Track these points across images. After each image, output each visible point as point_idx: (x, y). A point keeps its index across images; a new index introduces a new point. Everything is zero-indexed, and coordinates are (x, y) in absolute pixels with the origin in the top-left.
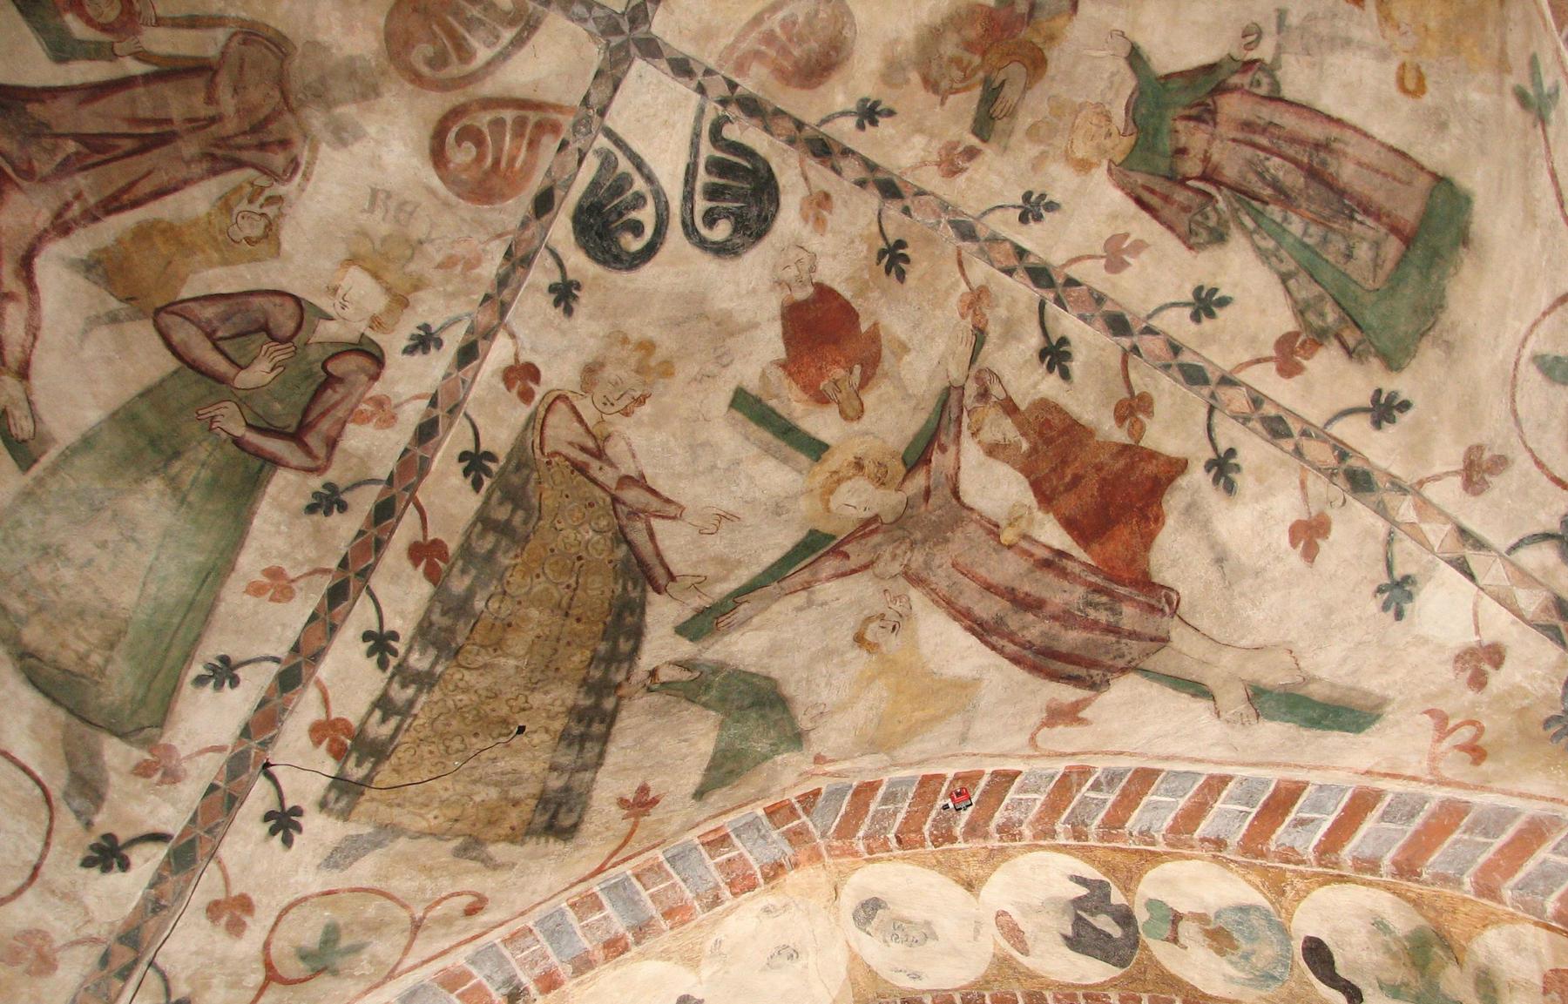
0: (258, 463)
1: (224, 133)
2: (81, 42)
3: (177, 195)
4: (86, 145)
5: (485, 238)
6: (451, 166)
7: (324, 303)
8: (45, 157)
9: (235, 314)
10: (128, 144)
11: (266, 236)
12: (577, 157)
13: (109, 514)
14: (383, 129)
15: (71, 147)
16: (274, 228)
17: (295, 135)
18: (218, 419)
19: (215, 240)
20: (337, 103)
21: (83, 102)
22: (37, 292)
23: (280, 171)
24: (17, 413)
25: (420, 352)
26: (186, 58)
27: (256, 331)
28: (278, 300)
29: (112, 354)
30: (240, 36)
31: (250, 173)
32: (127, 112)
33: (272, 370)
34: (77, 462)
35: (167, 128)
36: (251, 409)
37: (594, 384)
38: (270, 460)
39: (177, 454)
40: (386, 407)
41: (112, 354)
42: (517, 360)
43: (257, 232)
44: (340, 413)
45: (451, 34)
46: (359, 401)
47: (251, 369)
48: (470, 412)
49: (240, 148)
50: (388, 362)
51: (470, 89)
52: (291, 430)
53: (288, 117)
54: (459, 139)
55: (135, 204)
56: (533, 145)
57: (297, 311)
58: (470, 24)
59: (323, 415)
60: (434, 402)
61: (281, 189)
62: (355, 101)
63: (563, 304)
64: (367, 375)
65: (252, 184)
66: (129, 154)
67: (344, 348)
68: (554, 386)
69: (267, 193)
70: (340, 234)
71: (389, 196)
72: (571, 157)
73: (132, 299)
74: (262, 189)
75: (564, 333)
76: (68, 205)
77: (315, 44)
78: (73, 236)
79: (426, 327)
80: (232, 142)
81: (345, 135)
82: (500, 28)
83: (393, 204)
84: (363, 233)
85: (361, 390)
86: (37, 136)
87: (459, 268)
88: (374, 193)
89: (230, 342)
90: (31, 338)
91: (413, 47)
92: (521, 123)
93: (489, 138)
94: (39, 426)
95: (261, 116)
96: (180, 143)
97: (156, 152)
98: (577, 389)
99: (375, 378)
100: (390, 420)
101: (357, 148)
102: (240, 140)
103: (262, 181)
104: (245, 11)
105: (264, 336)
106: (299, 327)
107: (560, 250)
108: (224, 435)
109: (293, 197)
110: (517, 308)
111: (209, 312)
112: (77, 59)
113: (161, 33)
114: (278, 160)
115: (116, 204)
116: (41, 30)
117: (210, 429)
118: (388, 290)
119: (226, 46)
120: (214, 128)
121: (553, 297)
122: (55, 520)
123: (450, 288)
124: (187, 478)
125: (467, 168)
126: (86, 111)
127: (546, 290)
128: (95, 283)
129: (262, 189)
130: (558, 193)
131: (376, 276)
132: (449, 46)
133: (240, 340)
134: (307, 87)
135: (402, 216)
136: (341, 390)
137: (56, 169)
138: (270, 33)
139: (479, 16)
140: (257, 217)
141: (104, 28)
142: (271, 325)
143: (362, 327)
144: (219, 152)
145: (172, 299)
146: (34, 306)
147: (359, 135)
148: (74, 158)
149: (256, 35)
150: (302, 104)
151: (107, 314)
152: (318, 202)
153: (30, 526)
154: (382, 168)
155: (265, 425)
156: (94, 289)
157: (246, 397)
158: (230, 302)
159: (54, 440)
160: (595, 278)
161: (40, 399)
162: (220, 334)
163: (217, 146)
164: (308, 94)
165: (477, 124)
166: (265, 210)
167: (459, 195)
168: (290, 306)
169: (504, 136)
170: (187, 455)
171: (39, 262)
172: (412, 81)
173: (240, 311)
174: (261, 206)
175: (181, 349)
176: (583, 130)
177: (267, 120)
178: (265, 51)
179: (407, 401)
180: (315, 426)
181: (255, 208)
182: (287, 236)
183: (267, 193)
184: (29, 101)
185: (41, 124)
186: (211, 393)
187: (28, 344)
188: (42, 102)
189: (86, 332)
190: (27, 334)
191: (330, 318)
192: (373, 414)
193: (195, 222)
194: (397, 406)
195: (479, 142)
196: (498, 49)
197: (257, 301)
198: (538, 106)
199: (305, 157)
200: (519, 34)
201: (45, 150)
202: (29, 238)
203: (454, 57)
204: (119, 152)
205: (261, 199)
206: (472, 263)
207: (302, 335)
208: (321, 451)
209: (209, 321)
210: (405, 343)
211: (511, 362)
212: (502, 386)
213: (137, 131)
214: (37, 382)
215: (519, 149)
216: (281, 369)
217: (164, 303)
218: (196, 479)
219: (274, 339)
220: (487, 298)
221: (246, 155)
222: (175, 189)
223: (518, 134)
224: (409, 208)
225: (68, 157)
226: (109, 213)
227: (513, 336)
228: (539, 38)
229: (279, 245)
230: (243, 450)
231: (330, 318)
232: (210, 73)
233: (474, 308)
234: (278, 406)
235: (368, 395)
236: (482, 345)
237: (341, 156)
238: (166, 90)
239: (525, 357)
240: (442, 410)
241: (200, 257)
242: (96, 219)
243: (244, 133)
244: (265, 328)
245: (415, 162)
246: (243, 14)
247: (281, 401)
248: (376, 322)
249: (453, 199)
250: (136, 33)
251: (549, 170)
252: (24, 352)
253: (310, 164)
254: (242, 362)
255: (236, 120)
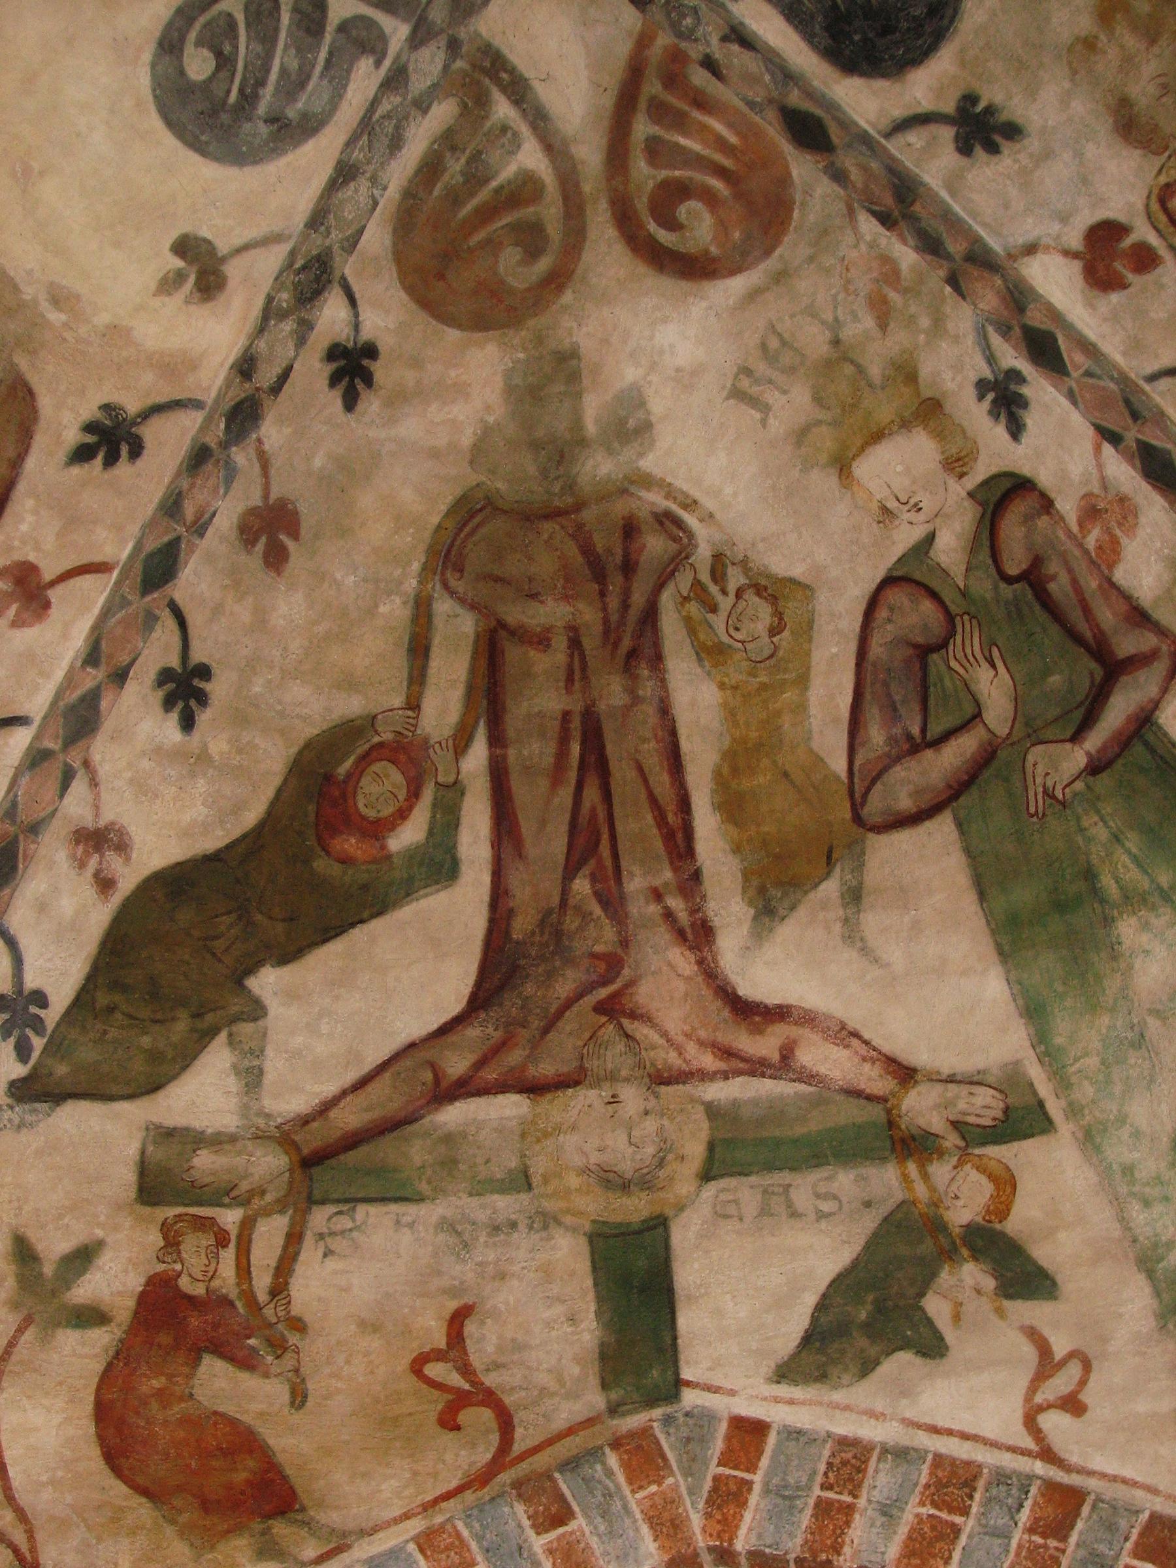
0: (1138, 748)
1: (598, 629)
2: (431, 833)
3: (683, 733)
4: (582, 862)
5: (850, 238)
6: (714, 250)
7: (905, 536)
8: (592, 931)
9: (889, 695)
10: (592, 794)
11: (774, 600)
12: (735, 48)
13: (1153, 1023)
14: (632, 354)
15: (582, 886)
16: (763, 582)
17: (620, 508)
18: (1049, 784)
19: (764, 687)
20: (577, 425)
21: (520, 854)
22: (789, 1007)
23: (674, 547)
24: (962, 1105)
25: (1021, 412)
26: (473, 670)
27: (924, 668)
28: (882, 614)
29: (906, 919)
30: (449, 574)
31: (667, 599)
32: (544, 784)
33: (993, 666)
34: (1059, 1040)
35: (576, 724)
36: (1047, 725)
37: (1156, 128)
38: (1141, 727)
39: (1089, 875)
40: (1101, 505)
41: (906, 919)
42: (1075, 255)
43: (764, 613)
44: (1091, 583)
45: (487, 213)
46: (1081, 546)
47: (983, 698)
48: (1149, 370)
49: (625, 606)
50: (1026, 471)
51: (587, 188)
52: (1099, 673)
53: (588, 515)
54: (673, 225)
55: (684, 804)
56: (701, 102)
57: (909, 588)
58: (475, 178)
59: (1086, 610)
60: (1113, 438)
61: (703, 553)
62: (579, 395)
63: (998, 139)
64: (1039, 515)
65: (686, 599)
66: (607, 796)
67: (986, 534)
68: (1140, 205)
69: (705, 577)
70: (796, 473)
71: (747, 371)
72: (736, 58)
73: (829, 857)
74: (697, 584)
75: (1047, 155)
76: (669, 915)
77: (478, 453)
78: (716, 922)
79: (982, 387)
80: (614, 618)
81: (631, 423)
82: (488, 124)
83: (761, 368)
84: (801, 435)
85: (1061, 534)
86: (558, 934)
87: (893, 296)
88: (737, 394)
89: (931, 719)
90: (855, 1042)
91: (502, 282)
92: (660, 112)
93: (677, 173)
94: (991, 1080)
95: (580, 559)
96: (602, 706)
97: (609, 748)
98: (1158, 161)
99: (1047, 504)
100: (1126, 509)
101: (657, 406)
102: (613, 603)
103: (684, 581)
104: (409, 563)
105: (935, 657)
106: (934, 595)
107: (898, 113)
108: (1079, 786)
109: (718, 536)
110: (985, 225)
111: (876, 736)
112: (455, 846)
113: (430, 705)
114: (655, 545)
115: (680, 836)
116: (407, 891)
117: (1063, 804)
118: (905, 425)
119: (462, 601)
120: (586, 642)
121: (979, 151)
122: (1139, 1111)
123: (925, 322)
124: (1133, 875)
125: (722, 226)
126: (532, 850)
127: (963, 161)
128: (793, 908)
129: (697, 584)
130: (795, 99)
131: (877, 436)
132: (507, 219)
133: (932, 702)
134: (544, 473)
135: (787, 358)
136: (1053, 567)
137: (612, 919)
138: (451, 525)
139: (463, 161)
140: (742, 604)
141: (414, 794)
142: (920, 640)
143: (958, 490)
144: (627, 643)
145: (844, 791)
146: (809, 1019)
147: (634, 399)
148: (599, 886)
149: (452, 545)
150: (570, 486)
151: (845, 906)
152: (735, 494)
153: (1136, 1155)
154: (697, 371)
155: (1082, 710)
156: (802, 912)
157: (1027, 724)
158: (868, 696)
159: (1017, 1063)
160: (963, 64)
161: (948, 1063)
162: (916, 731)
163: (616, 645)
164: (553, 474)
165: (651, 184)
166: (732, 587)
167: (768, 253)
168: (897, 596)
169: (677, 144)
170: (1094, 859)
171: (745, 990)
172: (560, 288)
173: (886, 684)
174: (724, 592)
175: (925, 802)
176: (688, 21)
177: (587, 550)
178: (475, 538)
179: (1100, 466)
180: (1102, 632)
181: (725, 603)
182: (780, 564)
183: (705, 577)
184: (507, 933)
185: (542, 923)
186: (1007, 780)
187: (863, 1050)
188: (511, 913)
189: (865, 950)
190: (847, 1047)
191: (930, 538)
192: (1108, 531)
193: (731, 714)
194: (1105, 487)
195: (681, 191)
196: (524, 130)
197: (876, 649)
198: (635, 72)
199: (656, 499)
200: (504, 90)
201: (581, 928)
202: (707, 993)
203: (528, 212)
204: (601, 814)
205: (714, 589)
206: (890, 273)
207: (948, 596)
208: (1147, 641)
209: (891, 740)
210: (1000, 431)
211: (1077, 266)
212: (1115, 297)
213: (572, 775)
214: (920, 1058)
215: (704, 128)
216: (995, 651)
217: (847, 805)
218: (1135, 859)
219: (943, 645)
220: (953, 280)
221: (638, 599)
222: (673, 733)
223: (679, 122)
224: (774, 343)
225: (597, 895)
226: (690, 852)
227: (1031, 249)
228: (518, 54)
229: (792, 581)
230: (1109, 764)
231: (930, 538)
232: (503, 633)
233: (966, 310)
234: (1055, 680)
235: (1075, 528)
236: (1035, 318)
237: (665, 436)
238: (518, 712)
239: (1074, 238)
240: (1127, 429)
241: (786, 721)
242: (697, 876)
243: (602, 594)
244: (924, 652)
245: (698, 309)
246: (416, 566)
247: (1047, 672)
248: (956, 465)
249: (771, 264)
250: (425, 744)
251: (751, 104)
252: (873, 1061)
253: (670, 492)
254: (969, 710)
255: (581, 606)
